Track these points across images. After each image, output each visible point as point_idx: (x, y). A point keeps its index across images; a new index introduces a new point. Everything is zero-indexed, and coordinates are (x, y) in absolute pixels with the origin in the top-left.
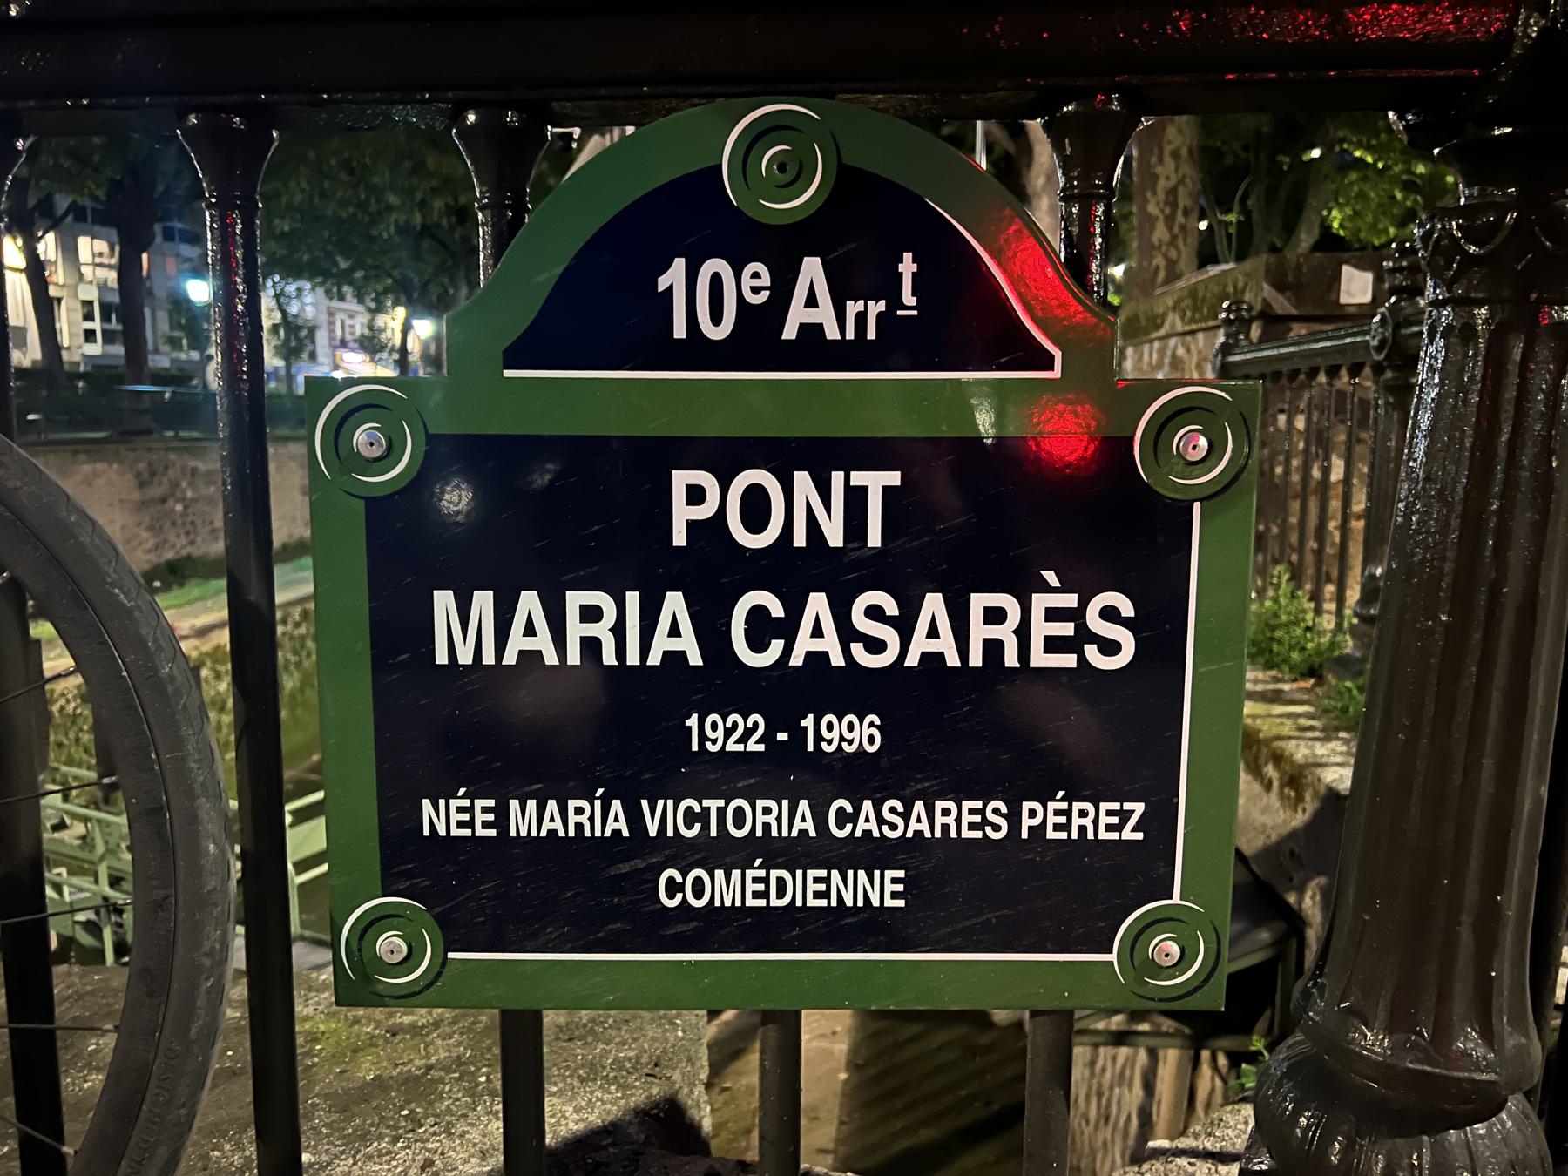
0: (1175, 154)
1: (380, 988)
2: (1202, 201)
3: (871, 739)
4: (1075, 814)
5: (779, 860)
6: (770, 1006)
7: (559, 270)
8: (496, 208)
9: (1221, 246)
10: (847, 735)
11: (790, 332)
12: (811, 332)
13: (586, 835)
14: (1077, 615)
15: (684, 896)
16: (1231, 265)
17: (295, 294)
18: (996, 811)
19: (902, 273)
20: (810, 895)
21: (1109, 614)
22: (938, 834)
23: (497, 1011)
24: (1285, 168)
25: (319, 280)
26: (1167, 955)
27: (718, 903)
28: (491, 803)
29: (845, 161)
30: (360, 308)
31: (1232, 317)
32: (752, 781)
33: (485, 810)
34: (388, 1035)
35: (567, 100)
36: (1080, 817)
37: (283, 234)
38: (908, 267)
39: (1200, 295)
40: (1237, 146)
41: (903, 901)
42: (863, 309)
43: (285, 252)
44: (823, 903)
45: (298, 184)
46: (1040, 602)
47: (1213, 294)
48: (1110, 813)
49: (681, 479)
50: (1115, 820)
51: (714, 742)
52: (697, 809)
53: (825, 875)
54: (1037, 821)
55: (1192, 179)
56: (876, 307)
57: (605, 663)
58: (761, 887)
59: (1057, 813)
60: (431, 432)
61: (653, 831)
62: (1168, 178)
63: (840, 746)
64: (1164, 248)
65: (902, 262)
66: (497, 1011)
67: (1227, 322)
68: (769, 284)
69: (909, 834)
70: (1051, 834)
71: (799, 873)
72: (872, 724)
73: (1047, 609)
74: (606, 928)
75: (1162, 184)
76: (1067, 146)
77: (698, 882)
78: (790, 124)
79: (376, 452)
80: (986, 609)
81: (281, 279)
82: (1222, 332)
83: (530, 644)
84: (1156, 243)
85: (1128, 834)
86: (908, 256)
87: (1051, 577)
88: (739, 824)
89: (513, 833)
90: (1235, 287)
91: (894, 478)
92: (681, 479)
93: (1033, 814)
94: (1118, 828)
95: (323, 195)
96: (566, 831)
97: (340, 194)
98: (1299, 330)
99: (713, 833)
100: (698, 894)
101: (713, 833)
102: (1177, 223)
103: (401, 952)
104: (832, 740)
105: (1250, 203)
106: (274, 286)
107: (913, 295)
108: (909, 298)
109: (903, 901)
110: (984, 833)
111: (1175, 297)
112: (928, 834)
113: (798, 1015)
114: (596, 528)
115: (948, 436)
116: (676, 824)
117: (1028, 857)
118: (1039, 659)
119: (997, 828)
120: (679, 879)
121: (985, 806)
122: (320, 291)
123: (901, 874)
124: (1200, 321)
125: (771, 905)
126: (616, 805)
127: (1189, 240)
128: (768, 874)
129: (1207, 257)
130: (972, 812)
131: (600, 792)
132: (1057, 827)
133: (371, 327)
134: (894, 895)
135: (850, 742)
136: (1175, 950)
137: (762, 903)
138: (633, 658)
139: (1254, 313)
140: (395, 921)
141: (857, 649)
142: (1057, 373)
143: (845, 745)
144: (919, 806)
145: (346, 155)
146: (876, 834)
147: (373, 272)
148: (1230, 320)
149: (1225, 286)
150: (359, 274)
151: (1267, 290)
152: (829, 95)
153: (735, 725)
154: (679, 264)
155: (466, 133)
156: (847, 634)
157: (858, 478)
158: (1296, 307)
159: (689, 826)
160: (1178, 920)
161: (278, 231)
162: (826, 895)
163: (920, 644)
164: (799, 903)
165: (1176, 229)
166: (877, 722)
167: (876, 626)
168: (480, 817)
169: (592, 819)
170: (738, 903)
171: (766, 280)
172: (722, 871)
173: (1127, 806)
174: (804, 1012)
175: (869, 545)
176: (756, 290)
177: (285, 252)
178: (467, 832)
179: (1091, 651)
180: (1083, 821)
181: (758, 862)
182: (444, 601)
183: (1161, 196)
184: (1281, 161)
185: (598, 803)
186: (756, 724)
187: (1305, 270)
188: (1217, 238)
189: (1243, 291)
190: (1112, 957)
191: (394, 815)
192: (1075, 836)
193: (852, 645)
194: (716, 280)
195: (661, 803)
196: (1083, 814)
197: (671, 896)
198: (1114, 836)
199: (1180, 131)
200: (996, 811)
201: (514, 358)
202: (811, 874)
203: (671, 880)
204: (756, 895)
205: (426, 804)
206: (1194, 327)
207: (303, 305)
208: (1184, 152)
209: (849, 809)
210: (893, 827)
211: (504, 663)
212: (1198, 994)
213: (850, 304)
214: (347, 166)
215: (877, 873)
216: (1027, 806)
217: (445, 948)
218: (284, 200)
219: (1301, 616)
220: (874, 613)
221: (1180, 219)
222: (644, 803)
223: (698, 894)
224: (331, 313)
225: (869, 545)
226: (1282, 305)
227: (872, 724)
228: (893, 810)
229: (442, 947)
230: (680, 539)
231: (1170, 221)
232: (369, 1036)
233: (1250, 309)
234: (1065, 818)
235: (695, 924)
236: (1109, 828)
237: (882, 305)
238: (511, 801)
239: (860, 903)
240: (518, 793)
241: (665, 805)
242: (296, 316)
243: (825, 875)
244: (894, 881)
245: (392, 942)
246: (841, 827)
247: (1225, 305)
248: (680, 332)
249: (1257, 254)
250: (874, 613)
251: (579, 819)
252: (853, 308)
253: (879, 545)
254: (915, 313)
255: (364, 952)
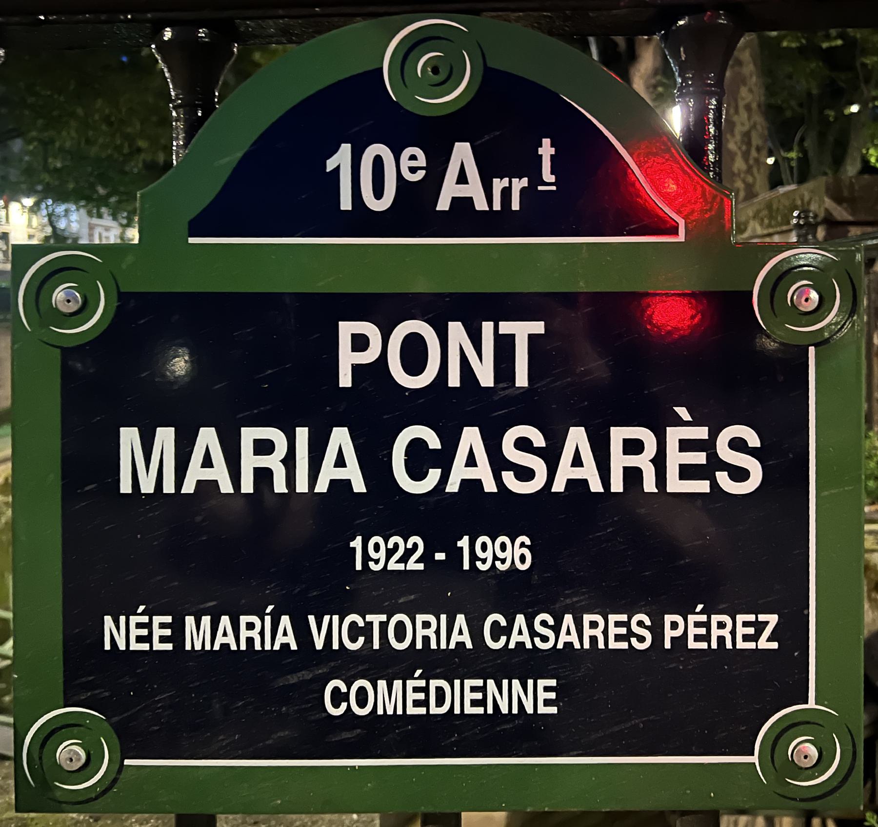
0: (748, 108)
1: (58, 794)
2: (770, 144)
3: (523, 559)
4: (714, 625)
5: (438, 671)
6: (430, 809)
7: (239, 155)
8: (188, 107)
9: (785, 175)
10: (500, 555)
11: (443, 204)
12: (462, 204)
13: (256, 648)
14: (708, 446)
15: (349, 706)
16: (793, 187)
17: (63, 213)
18: (640, 624)
19: (541, 156)
20: (467, 703)
21: (737, 445)
22: (587, 645)
23: (173, 815)
24: (831, 119)
25: (83, 203)
26: (806, 757)
27: (380, 712)
28: (168, 619)
29: (490, 64)
30: (114, 224)
31: (801, 222)
32: (412, 597)
33: (162, 626)
34: (91, 820)
35: (249, 19)
36: (718, 628)
37: (56, 170)
38: (546, 150)
39: (775, 207)
40: (793, 103)
41: (556, 708)
42: (508, 185)
43: (57, 183)
44: (480, 710)
45: (69, 133)
46: (674, 435)
47: (785, 206)
48: (746, 624)
49: (347, 329)
50: (751, 631)
51: (377, 562)
52: (361, 624)
53: (482, 685)
54: (678, 633)
55: (762, 127)
56: (519, 184)
57: (276, 491)
58: (421, 696)
59: (697, 625)
60: (122, 290)
61: (319, 644)
62: (743, 124)
63: (493, 565)
64: (742, 175)
65: (541, 146)
66: (173, 815)
67: (798, 226)
68: (425, 165)
69: (560, 646)
70: (692, 645)
71: (457, 682)
72: (523, 545)
73: (681, 441)
74: (275, 736)
75: (739, 129)
76: (682, 53)
77: (362, 691)
78: (442, 36)
79: (73, 307)
80: (625, 441)
81: (54, 202)
82: (794, 234)
83: (207, 474)
84: (736, 171)
85: (763, 643)
86: (546, 142)
87: (683, 412)
88: (400, 637)
89: (188, 647)
90: (802, 200)
91: (538, 327)
92: (347, 329)
93: (674, 626)
94: (755, 638)
95: (88, 142)
96: (238, 645)
97: (101, 140)
98: (854, 231)
99: (376, 646)
100: (362, 703)
101: (376, 646)
102: (751, 157)
103: (79, 759)
104: (486, 559)
105: (806, 144)
106: (47, 208)
107: (552, 174)
108: (548, 176)
109: (556, 708)
110: (630, 644)
111: (755, 209)
112: (577, 646)
113: (458, 816)
114: (270, 371)
115: (585, 291)
116: (342, 638)
117: (671, 666)
118: (675, 485)
119: (641, 639)
120: (344, 689)
121: (630, 619)
122: (83, 211)
123: (553, 683)
124: (776, 226)
125: (431, 712)
126: (285, 621)
127: (762, 170)
128: (428, 684)
129: (775, 179)
130: (618, 624)
131: (270, 608)
132: (697, 638)
133: (122, 238)
134: (547, 703)
135: (503, 561)
136: (813, 751)
137: (422, 711)
138: (302, 486)
139: (819, 219)
140: (76, 730)
141: (508, 477)
142: (681, 237)
143: (498, 563)
144: (568, 619)
145: (107, 111)
146: (529, 646)
147: (124, 198)
148: (800, 225)
149: (794, 200)
150: (113, 200)
151: (828, 203)
152: (477, 12)
153: (396, 546)
154: (346, 149)
155: (163, 47)
156: (499, 463)
157: (506, 327)
158: (852, 215)
159: (353, 640)
160: (814, 723)
161: (52, 167)
162: (483, 703)
163: (565, 472)
164: (457, 711)
165: (751, 162)
166: (528, 542)
167: (523, 456)
168: (157, 632)
169: (262, 634)
170: (400, 712)
171: (422, 161)
172: (385, 682)
173: (762, 618)
174: (463, 814)
175: (517, 385)
176: (413, 170)
177: (57, 183)
178: (145, 647)
179: (722, 477)
180: (721, 632)
181: (418, 673)
182: (129, 437)
183: (738, 137)
184: (828, 115)
185: (268, 619)
186: (415, 545)
187: (857, 188)
188: (782, 169)
189: (809, 203)
190: (754, 759)
191: (77, 630)
192: (714, 645)
193: (503, 473)
194: (378, 162)
195: (327, 618)
196: (721, 625)
197: (336, 705)
198: (751, 645)
199: (751, 91)
200: (640, 624)
201: (198, 227)
202: (468, 683)
203: (336, 690)
204: (416, 703)
205: (108, 620)
206: (771, 230)
207: (70, 221)
208: (754, 106)
209: (503, 623)
210: (545, 639)
211: (182, 492)
212: (837, 794)
213: (496, 181)
214: (107, 120)
215: (530, 682)
216: (668, 619)
217: (121, 755)
218: (57, 144)
219: (874, 452)
220: (523, 444)
221: (754, 153)
222: (311, 619)
223: (362, 703)
224: (91, 228)
225: (517, 385)
226: (841, 213)
227: (523, 545)
228: (544, 623)
229: (119, 754)
230: (345, 380)
231: (746, 156)
232: (74, 821)
233: (816, 216)
234: (704, 629)
235: (359, 731)
236: (746, 638)
237: (525, 182)
238: (187, 617)
239: (515, 711)
240: (194, 610)
241: (331, 620)
242: (63, 230)
243: (482, 685)
244: (547, 689)
245: (71, 750)
246: (495, 639)
247: (795, 214)
248: (346, 204)
249: (814, 177)
250: (523, 444)
251: (250, 634)
252: (499, 185)
253: (526, 385)
254: (554, 188)
255: (45, 760)
